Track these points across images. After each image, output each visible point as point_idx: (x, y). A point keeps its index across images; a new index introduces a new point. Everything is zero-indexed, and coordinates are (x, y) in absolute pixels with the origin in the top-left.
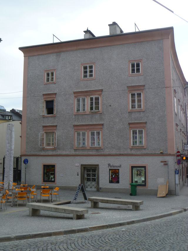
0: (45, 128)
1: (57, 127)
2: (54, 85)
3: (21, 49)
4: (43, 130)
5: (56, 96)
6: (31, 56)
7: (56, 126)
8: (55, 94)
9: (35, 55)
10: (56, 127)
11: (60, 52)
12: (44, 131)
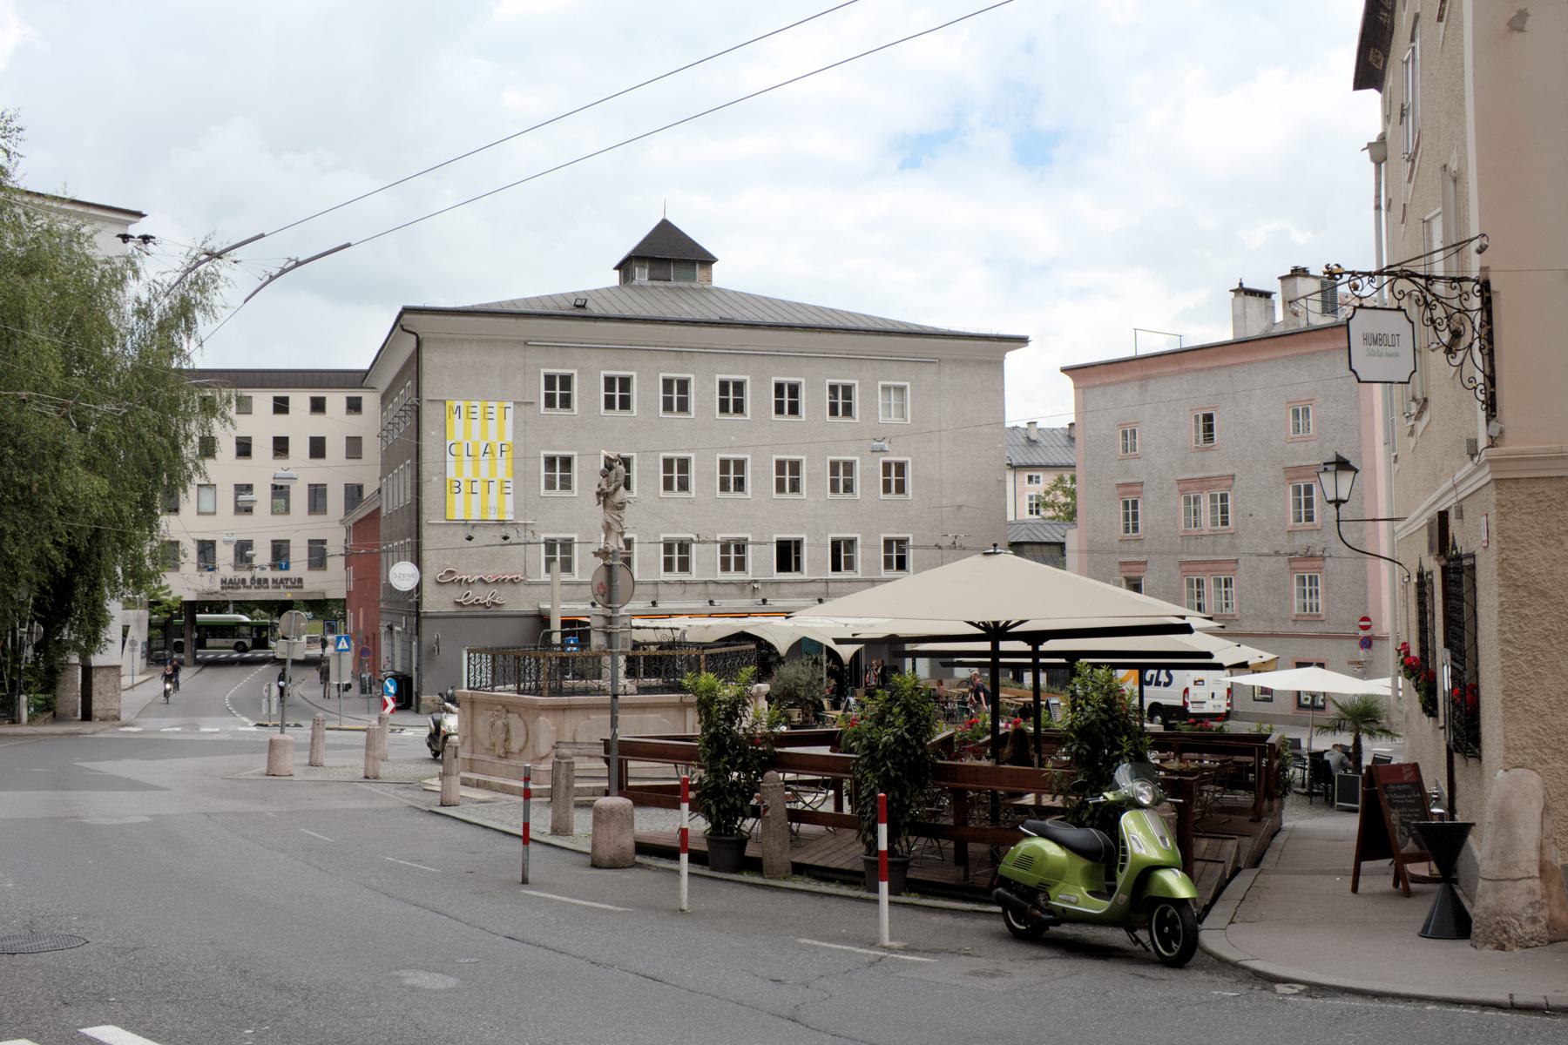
0: (1124, 568)
2: (1137, 462)
6: (1088, 387)
7: (1145, 563)
8: (1141, 484)
9: (1097, 386)
12: (1123, 574)
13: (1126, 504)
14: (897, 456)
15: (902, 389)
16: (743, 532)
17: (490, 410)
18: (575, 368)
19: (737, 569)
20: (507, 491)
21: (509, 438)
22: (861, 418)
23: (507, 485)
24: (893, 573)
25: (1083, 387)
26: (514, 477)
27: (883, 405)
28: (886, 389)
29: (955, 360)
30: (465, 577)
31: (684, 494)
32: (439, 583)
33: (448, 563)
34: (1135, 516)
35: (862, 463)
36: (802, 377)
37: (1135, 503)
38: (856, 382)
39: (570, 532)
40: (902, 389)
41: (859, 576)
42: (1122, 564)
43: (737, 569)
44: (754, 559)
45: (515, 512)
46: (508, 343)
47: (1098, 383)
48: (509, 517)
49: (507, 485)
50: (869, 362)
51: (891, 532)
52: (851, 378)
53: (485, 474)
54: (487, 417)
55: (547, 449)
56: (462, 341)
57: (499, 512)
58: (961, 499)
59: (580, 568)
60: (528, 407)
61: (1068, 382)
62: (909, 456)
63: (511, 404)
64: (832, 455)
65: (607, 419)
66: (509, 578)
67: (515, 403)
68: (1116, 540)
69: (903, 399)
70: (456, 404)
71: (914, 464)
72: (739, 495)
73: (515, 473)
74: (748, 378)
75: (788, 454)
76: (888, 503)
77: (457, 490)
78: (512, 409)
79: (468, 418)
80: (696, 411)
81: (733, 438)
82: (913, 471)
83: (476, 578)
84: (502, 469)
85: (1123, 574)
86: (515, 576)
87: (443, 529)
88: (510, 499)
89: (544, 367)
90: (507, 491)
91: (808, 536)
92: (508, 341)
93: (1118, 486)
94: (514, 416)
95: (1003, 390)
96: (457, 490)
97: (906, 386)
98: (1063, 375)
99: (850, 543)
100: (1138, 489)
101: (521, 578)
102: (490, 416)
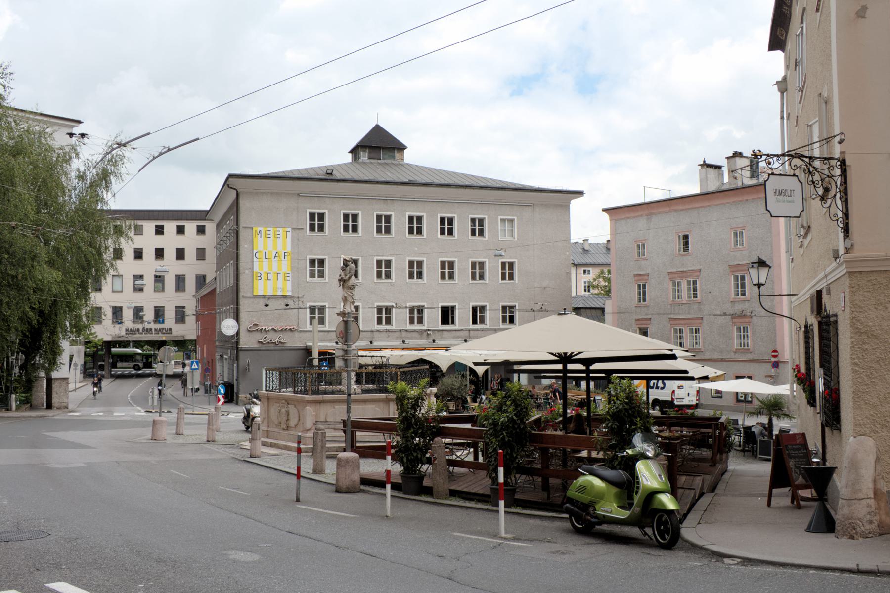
0: (638, 322)
2: (645, 262)
6: (618, 220)
7: (650, 319)
8: (648, 275)
9: (622, 219)
12: (637, 326)
13: (639, 286)
14: (509, 259)
15: (512, 221)
16: (422, 302)
17: (278, 233)
18: (326, 209)
19: (418, 323)
20: (288, 278)
21: (289, 249)
22: (488, 237)
23: (288, 275)
24: (507, 325)
25: (615, 220)
26: (292, 271)
27: (501, 230)
28: (503, 221)
29: (542, 204)
30: (264, 328)
31: (388, 281)
32: (249, 331)
33: (254, 320)
34: (644, 293)
35: (489, 263)
36: (455, 214)
37: (644, 286)
38: (486, 217)
39: (324, 302)
40: (512, 221)
41: (488, 327)
42: (637, 320)
43: (418, 323)
44: (428, 317)
45: (292, 291)
46: (289, 195)
47: (623, 217)
48: (289, 293)
49: (288, 275)
50: (493, 206)
51: (506, 302)
52: (483, 215)
53: (275, 269)
54: (277, 236)
55: (311, 255)
56: (262, 193)
57: (283, 291)
58: (545, 283)
59: (329, 323)
60: (300, 231)
61: (606, 217)
62: (516, 259)
63: (290, 229)
64: (472, 258)
65: (344, 238)
66: (289, 328)
67: (292, 229)
68: (634, 306)
69: (512, 226)
70: (259, 229)
71: (519, 263)
72: (419, 281)
73: (292, 268)
74: (424, 215)
75: (447, 257)
76: (504, 285)
77: (259, 278)
78: (291, 232)
79: (265, 237)
80: (395, 233)
81: (416, 249)
82: (518, 267)
83: (270, 328)
84: (285, 266)
85: (637, 326)
86: (292, 327)
87: (252, 300)
88: (289, 283)
89: (309, 208)
90: (288, 278)
91: (459, 304)
92: (288, 194)
93: (635, 276)
94: (292, 236)
95: (569, 221)
96: (259, 278)
97: (514, 219)
98: (603, 213)
99: (483, 308)
100: (646, 277)
101: (296, 328)
102: (278, 236)
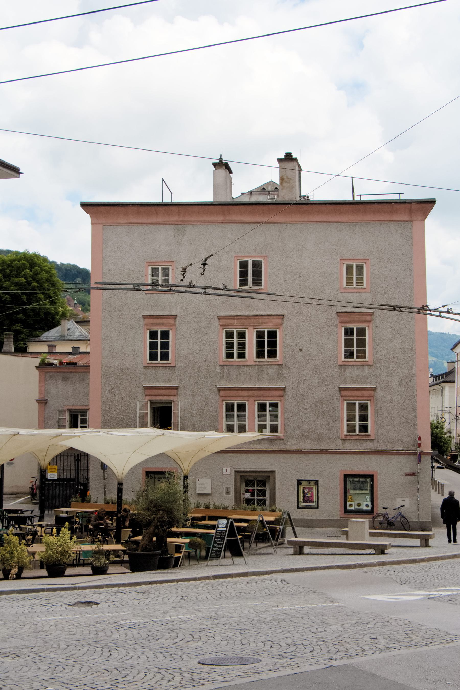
1: (180, 390)
3: (85, 205)
4: (146, 395)
5: (175, 322)
7: (177, 388)
8: (175, 317)
9: (120, 224)
10: (177, 389)
11: (184, 223)
12: (148, 398)
13: (153, 335)
37: (165, 335)
61: (86, 218)
93: (145, 317)
